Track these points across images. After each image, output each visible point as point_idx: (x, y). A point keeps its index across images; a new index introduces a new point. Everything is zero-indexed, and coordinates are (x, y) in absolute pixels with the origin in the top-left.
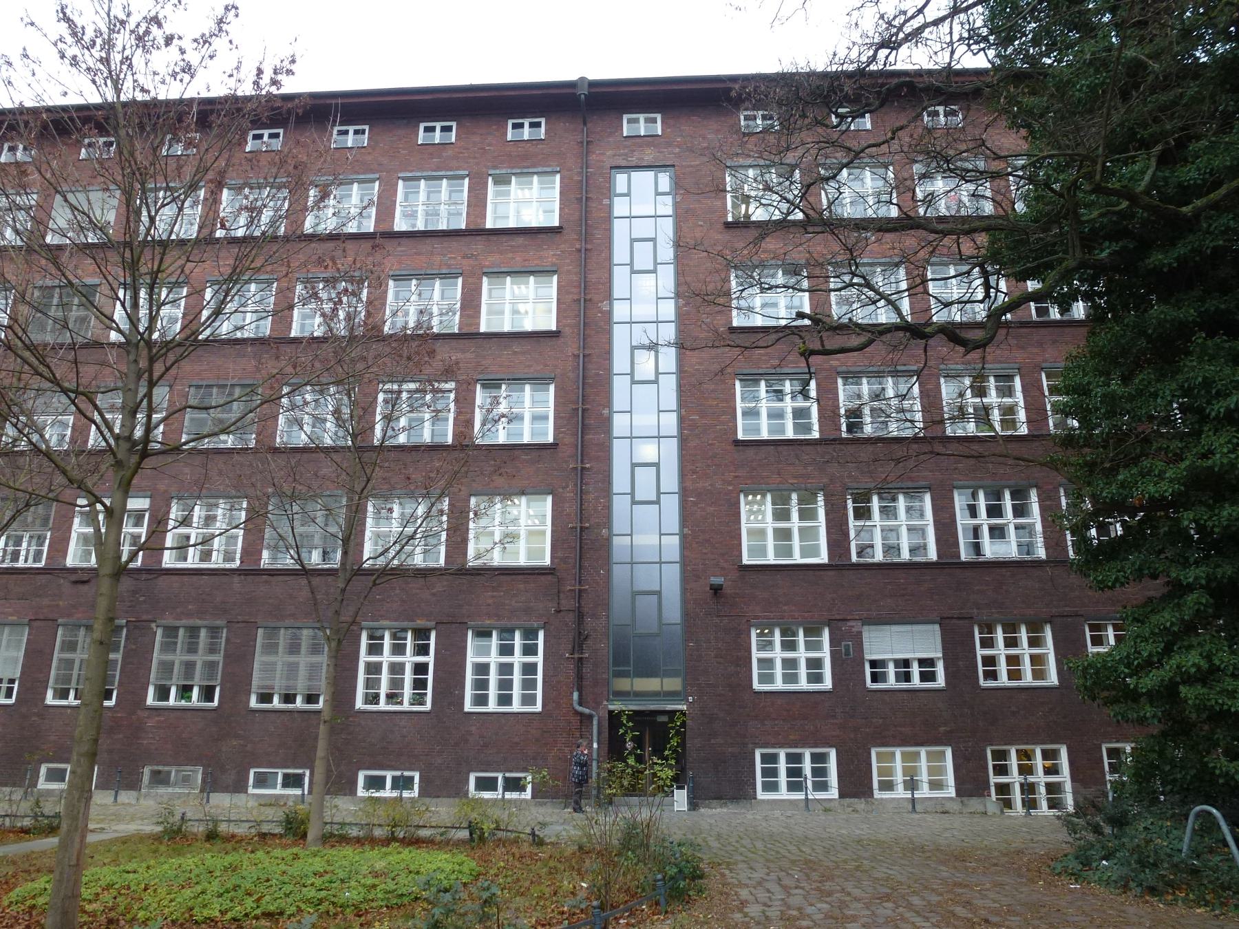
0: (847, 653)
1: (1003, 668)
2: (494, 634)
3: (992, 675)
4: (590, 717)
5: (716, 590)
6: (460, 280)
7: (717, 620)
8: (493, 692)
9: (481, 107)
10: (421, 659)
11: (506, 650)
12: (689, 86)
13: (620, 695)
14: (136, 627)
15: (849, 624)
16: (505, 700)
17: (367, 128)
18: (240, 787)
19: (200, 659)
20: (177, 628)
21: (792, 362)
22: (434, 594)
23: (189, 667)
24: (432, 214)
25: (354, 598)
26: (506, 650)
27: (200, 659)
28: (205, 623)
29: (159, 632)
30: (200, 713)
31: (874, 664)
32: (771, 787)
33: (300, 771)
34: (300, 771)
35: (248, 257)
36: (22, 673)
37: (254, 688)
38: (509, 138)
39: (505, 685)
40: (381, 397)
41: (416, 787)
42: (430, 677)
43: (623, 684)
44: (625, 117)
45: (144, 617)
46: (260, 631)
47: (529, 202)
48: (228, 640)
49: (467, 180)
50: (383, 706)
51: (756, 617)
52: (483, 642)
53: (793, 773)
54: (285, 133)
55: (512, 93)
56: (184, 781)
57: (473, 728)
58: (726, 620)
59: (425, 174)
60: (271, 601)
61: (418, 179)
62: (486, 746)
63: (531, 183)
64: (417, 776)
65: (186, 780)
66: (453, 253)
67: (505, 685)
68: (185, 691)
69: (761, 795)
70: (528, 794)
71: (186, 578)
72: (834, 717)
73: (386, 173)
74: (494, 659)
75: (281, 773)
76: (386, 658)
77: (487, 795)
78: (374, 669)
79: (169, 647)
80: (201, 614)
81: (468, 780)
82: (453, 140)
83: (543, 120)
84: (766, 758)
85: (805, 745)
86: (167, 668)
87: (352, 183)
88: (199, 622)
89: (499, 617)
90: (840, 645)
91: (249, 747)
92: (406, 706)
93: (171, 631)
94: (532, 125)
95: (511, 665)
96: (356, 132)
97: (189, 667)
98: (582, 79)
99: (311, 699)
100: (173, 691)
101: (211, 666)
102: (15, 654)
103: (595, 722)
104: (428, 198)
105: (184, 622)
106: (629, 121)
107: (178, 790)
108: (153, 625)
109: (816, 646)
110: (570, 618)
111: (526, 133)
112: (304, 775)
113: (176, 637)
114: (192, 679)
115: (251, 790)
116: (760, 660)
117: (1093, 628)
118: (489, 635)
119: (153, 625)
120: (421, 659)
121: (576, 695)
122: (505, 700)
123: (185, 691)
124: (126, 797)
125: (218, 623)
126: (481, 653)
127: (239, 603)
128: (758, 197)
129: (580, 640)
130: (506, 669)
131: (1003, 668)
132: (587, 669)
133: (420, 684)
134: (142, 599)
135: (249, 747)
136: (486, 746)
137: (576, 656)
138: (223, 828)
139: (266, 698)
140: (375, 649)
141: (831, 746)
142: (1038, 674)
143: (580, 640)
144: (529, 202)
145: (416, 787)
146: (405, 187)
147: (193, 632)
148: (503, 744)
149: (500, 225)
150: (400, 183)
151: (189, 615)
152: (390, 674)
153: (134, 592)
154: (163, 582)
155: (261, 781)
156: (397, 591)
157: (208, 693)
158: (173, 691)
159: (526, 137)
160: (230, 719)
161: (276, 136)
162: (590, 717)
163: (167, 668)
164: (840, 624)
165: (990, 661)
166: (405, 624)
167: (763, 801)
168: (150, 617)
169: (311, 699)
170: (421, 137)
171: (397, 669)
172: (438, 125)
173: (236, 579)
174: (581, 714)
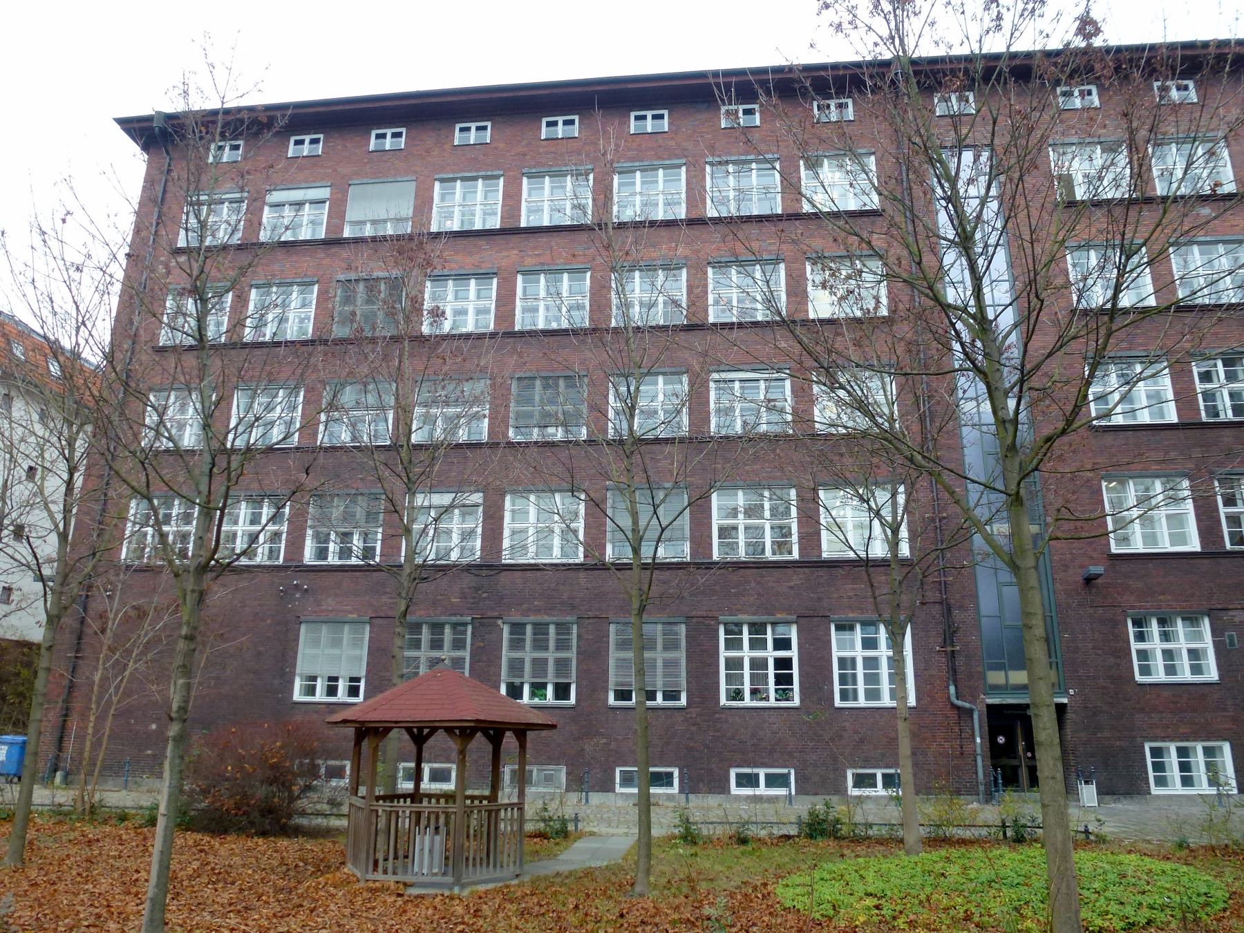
0: (1232, 644)
1: (1159, 663)
2: (858, 627)
3: (1145, 670)
4: (971, 711)
5: (1089, 580)
6: (589, 274)
7: (1091, 611)
8: (885, 686)
9: (688, 94)
10: (733, 654)
11: (870, 644)
12: (463, 98)
13: (995, 689)
14: (482, 625)
15: (1231, 613)
16: (873, 694)
17: (666, 113)
18: (721, 787)
19: (551, 655)
20: (524, 625)
21: (1141, 345)
22: (791, 588)
23: (540, 665)
24: (468, 213)
25: (711, 593)
26: (870, 644)
27: (551, 655)
28: (555, 619)
29: (506, 630)
30: (558, 711)
31: (842, 662)
32: (1161, 782)
33: (785, 771)
34: (785, 771)
35: (737, 237)
36: (368, 671)
37: (611, 686)
38: (372, 148)
39: (872, 679)
40: (712, 385)
41: (676, 781)
42: (795, 671)
43: (996, 677)
44: (458, 126)
45: (490, 614)
46: (612, 628)
47: (838, 187)
48: (579, 636)
49: (684, 169)
50: (748, 702)
51: (1132, 607)
52: (846, 635)
53: (1185, 767)
54: (245, 145)
55: (541, 92)
56: (546, 780)
57: (847, 724)
58: (1100, 611)
59: (733, 158)
60: (621, 596)
61: (475, 179)
62: (862, 741)
63: (454, 188)
64: (676, 773)
65: (549, 779)
66: (491, 256)
67: (872, 679)
68: (538, 688)
69: (1155, 791)
70: (675, 789)
71: (529, 574)
72: (1225, 710)
73: (514, 171)
74: (859, 653)
75: (879, 774)
76: (746, 654)
77: (867, 792)
78: (734, 664)
79: (517, 644)
80: (549, 610)
81: (845, 777)
82: (758, 123)
83: (666, 113)
84: (1157, 752)
85: (1197, 738)
86: (516, 666)
87: (634, 172)
88: (546, 618)
89: (862, 610)
90: (1223, 635)
91: (613, 746)
92: (772, 702)
93: (517, 628)
94: (566, 123)
95: (545, 661)
96: (478, 129)
97: (540, 665)
98: (158, 113)
99: (671, 695)
100: (526, 689)
101: (562, 665)
102: (358, 652)
103: (976, 716)
104: (464, 199)
105: (532, 618)
106: (637, 118)
107: (541, 790)
108: (500, 622)
109: (1199, 636)
110: (936, 610)
111: (649, 125)
112: (789, 774)
113: (443, 634)
114: (546, 676)
115: (618, 789)
116: (1138, 652)
117: (1137, 623)
118: (852, 628)
119: (500, 622)
120: (733, 654)
121: (952, 689)
122: (873, 694)
123: (538, 688)
124: (596, 798)
125: (569, 618)
126: (846, 646)
127: (587, 595)
128: (1089, 170)
129: (949, 635)
130: (871, 663)
131: (1159, 663)
132: (960, 661)
133: (783, 680)
134: (485, 595)
135: (613, 746)
136: (862, 741)
137: (949, 649)
138: (753, 831)
139: (623, 695)
140: (734, 644)
141: (1225, 740)
142: (1196, 669)
143: (949, 635)
144: (838, 187)
145: (676, 781)
146: (442, 189)
147: (437, 628)
148: (868, 738)
149: (534, 222)
150: (437, 185)
151: (538, 611)
152: (748, 670)
153: (477, 589)
154: (504, 578)
155: (748, 781)
156: (753, 585)
157: (562, 691)
158: (526, 689)
159: (388, 147)
160: (589, 718)
161: (399, 135)
162: (971, 711)
163: (516, 666)
164: (1222, 613)
165: (1143, 655)
166: (764, 618)
167: (1158, 796)
168: (496, 614)
169: (671, 695)
170: (633, 126)
171: (759, 664)
172: (389, 132)
173: (582, 574)
174: (958, 708)
